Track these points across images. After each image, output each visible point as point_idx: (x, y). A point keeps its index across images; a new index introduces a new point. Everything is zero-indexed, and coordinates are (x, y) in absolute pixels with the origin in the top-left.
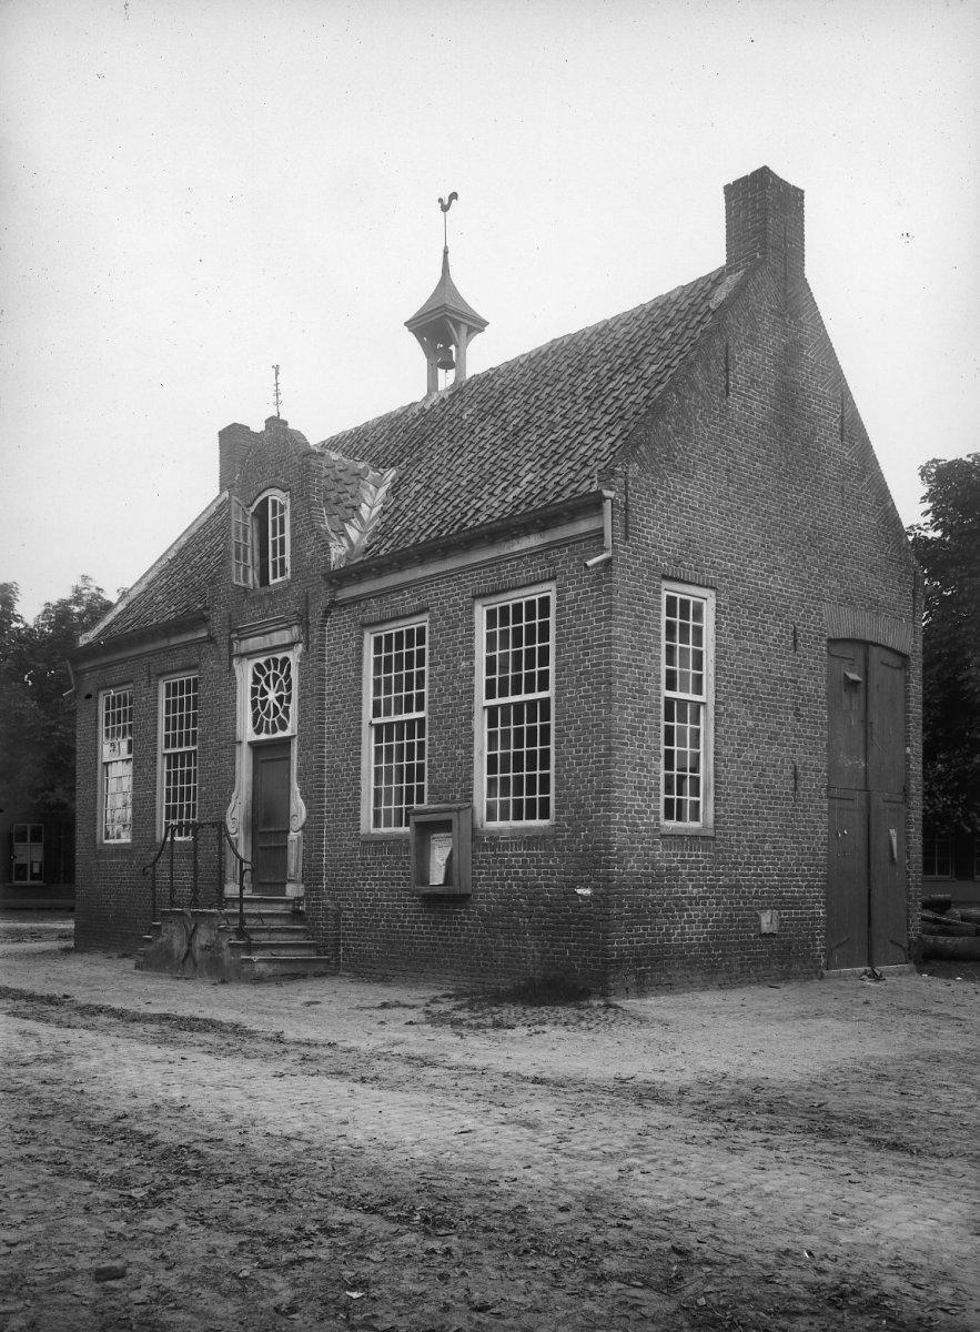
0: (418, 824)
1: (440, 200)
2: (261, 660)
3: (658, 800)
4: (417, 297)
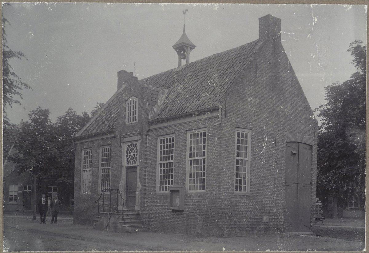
0: (171, 191)
1: (183, 11)
2: (129, 144)
3: (233, 186)
4: (176, 40)
